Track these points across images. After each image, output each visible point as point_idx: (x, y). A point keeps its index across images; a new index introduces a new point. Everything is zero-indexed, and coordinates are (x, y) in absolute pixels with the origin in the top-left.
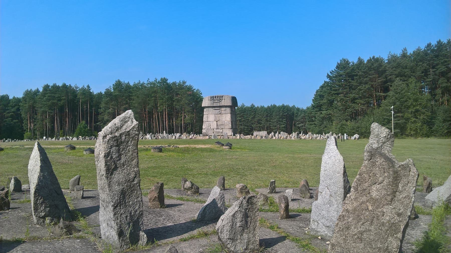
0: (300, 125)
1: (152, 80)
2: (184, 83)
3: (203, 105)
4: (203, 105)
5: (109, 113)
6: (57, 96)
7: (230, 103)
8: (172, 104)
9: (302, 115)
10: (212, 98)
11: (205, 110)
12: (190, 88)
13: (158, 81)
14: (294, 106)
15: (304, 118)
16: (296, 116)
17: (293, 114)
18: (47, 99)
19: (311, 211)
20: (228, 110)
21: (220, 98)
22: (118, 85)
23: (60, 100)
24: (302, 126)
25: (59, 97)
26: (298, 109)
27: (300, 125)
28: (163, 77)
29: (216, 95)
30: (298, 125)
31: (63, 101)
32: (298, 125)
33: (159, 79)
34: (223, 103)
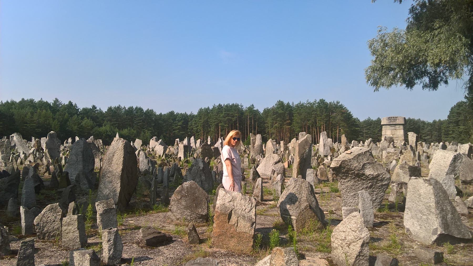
0: (426, 138)
1: (312, 101)
2: (338, 103)
3: (382, 124)
4: (382, 124)
5: (276, 127)
6: (231, 113)
7: (403, 123)
8: (329, 120)
9: (429, 128)
10: (389, 118)
11: (383, 127)
12: (341, 107)
13: (317, 102)
14: (419, 119)
15: (430, 131)
16: (423, 129)
17: (419, 127)
18: (223, 116)
19: (402, 208)
20: (402, 127)
21: (395, 118)
22: (281, 104)
23: (233, 117)
24: (429, 138)
25: (232, 114)
26: (423, 122)
27: (426, 138)
28: (321, 99)
29: (392, 116)
30: (424, 138)
31: (235, 117)
32: (424, 138)
33: (318, 100)
34: (398, 122)
